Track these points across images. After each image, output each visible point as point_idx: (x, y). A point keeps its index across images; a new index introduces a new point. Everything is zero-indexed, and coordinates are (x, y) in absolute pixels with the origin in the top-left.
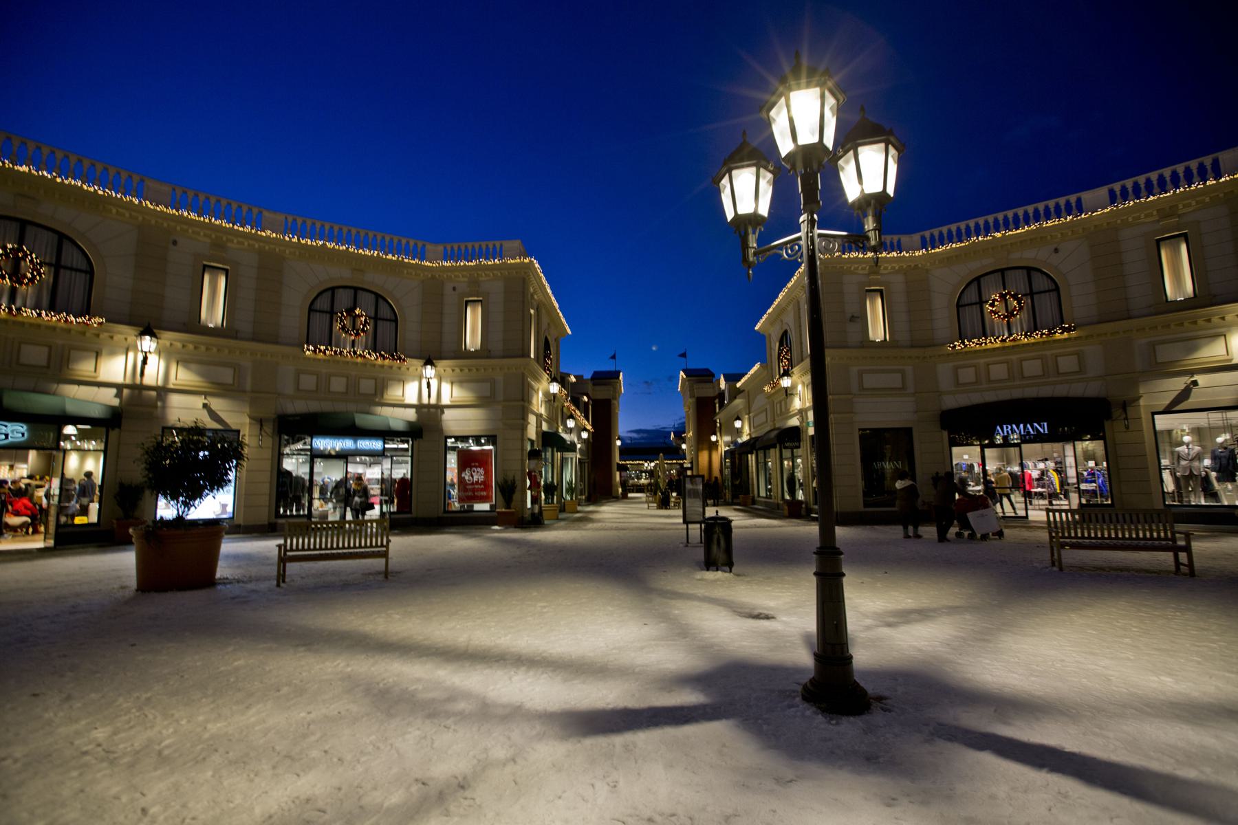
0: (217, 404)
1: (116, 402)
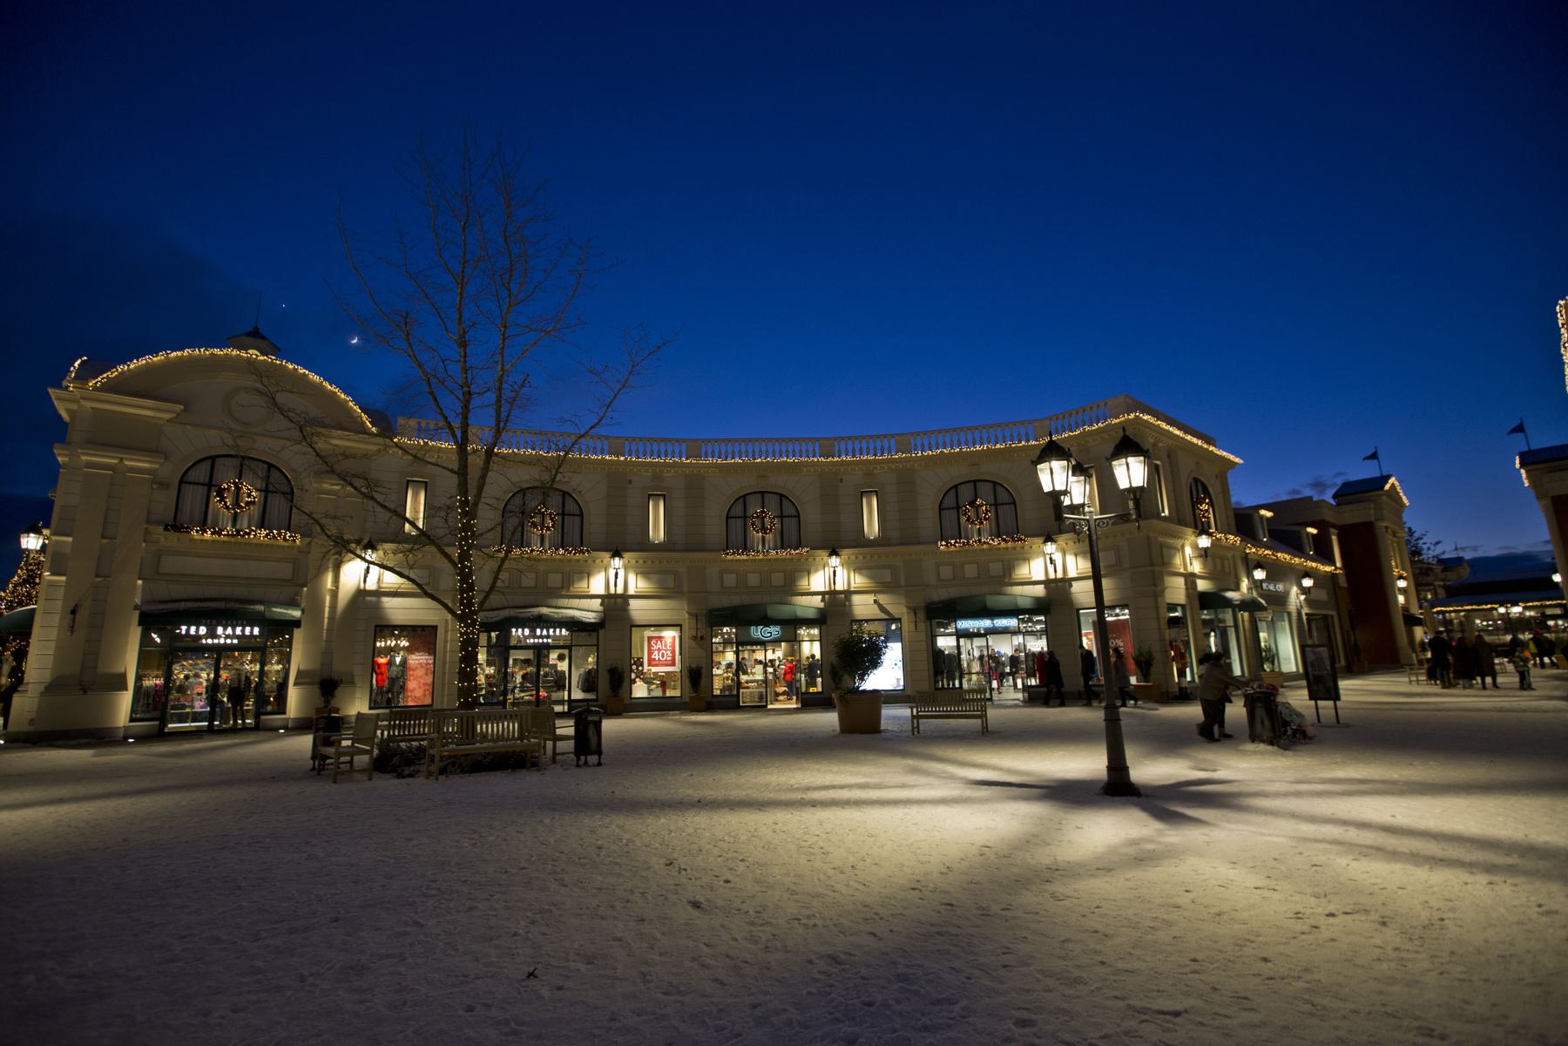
0: (882, 599)
1: (822, 605)
